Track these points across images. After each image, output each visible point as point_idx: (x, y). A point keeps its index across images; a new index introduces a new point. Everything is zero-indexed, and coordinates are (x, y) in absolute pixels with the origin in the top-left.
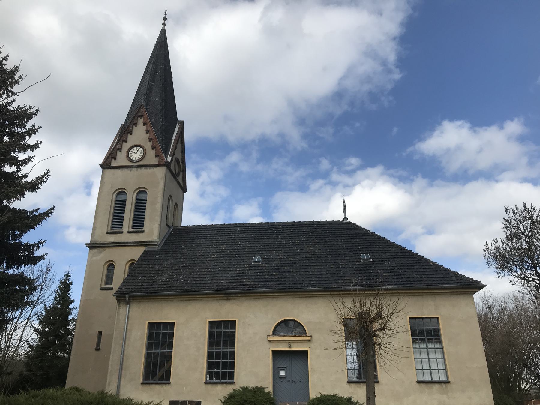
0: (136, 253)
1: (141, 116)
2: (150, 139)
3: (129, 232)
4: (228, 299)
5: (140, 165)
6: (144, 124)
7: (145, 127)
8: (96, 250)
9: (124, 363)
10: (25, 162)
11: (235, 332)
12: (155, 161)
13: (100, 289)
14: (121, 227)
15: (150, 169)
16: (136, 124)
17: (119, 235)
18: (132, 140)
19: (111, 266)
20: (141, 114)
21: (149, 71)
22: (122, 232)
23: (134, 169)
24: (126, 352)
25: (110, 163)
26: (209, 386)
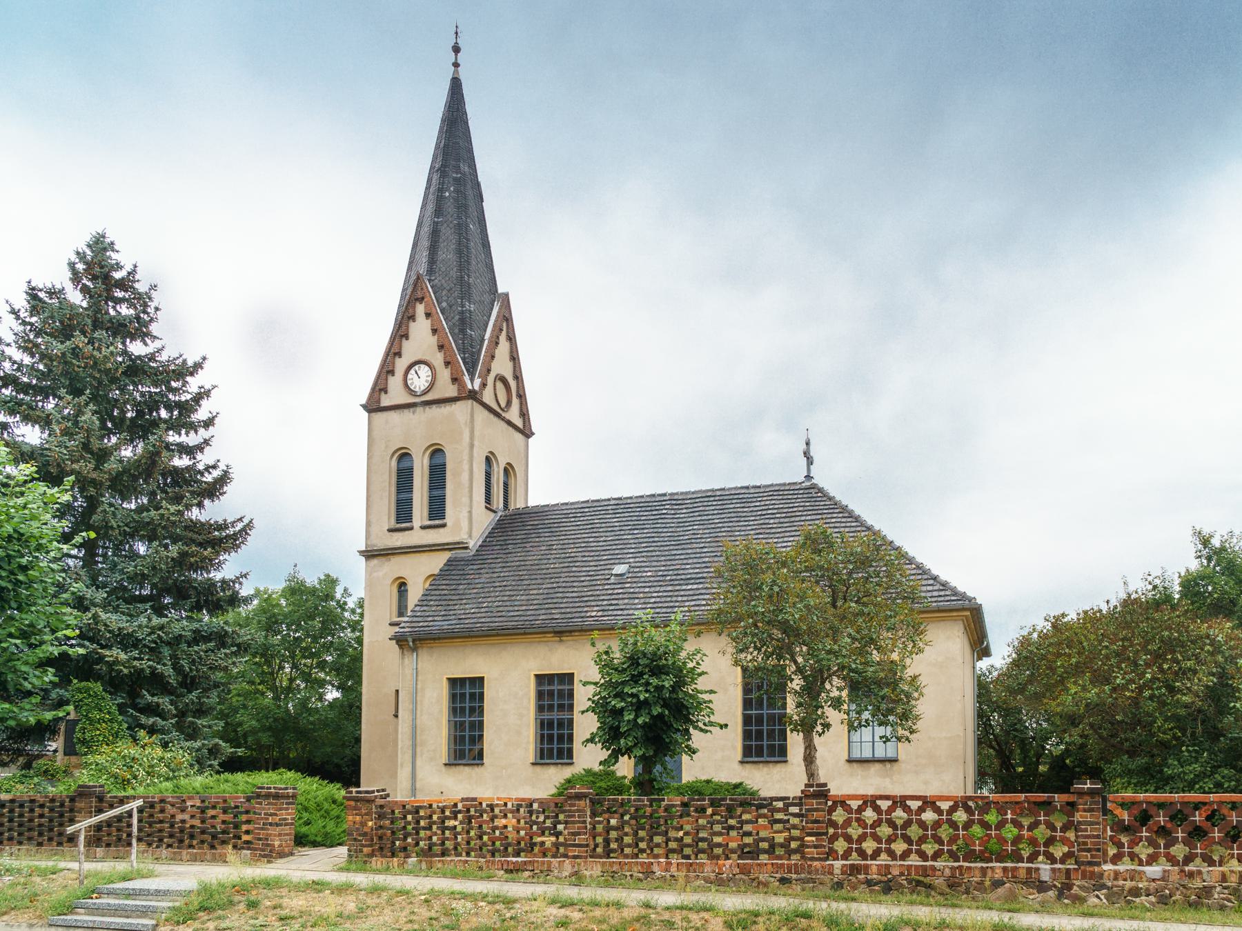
0: (436, 562)
1: (421, 300)
2: (441, 347)
3: (423, 528)
4: (561, 641)
5: (427, 401)
6: (428, 315)
7: (429, 321)
8: (375, 562)
9: (418, 738)
10: (199, 448)
11: (573, 690)
12: (452, 391)
13: (390, 624)
14: (409, 518)
15: (445, 407)
16: (412, 318)
17: (407, 532)
18: (410, 351)
19: (402, 586)
20: (419, 295)
21: (432, 190)
22: (411, 528)
23: (420, 409)
24: (418, 722)
25: (379, 401)
26: (538, 769)
